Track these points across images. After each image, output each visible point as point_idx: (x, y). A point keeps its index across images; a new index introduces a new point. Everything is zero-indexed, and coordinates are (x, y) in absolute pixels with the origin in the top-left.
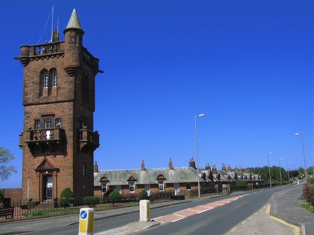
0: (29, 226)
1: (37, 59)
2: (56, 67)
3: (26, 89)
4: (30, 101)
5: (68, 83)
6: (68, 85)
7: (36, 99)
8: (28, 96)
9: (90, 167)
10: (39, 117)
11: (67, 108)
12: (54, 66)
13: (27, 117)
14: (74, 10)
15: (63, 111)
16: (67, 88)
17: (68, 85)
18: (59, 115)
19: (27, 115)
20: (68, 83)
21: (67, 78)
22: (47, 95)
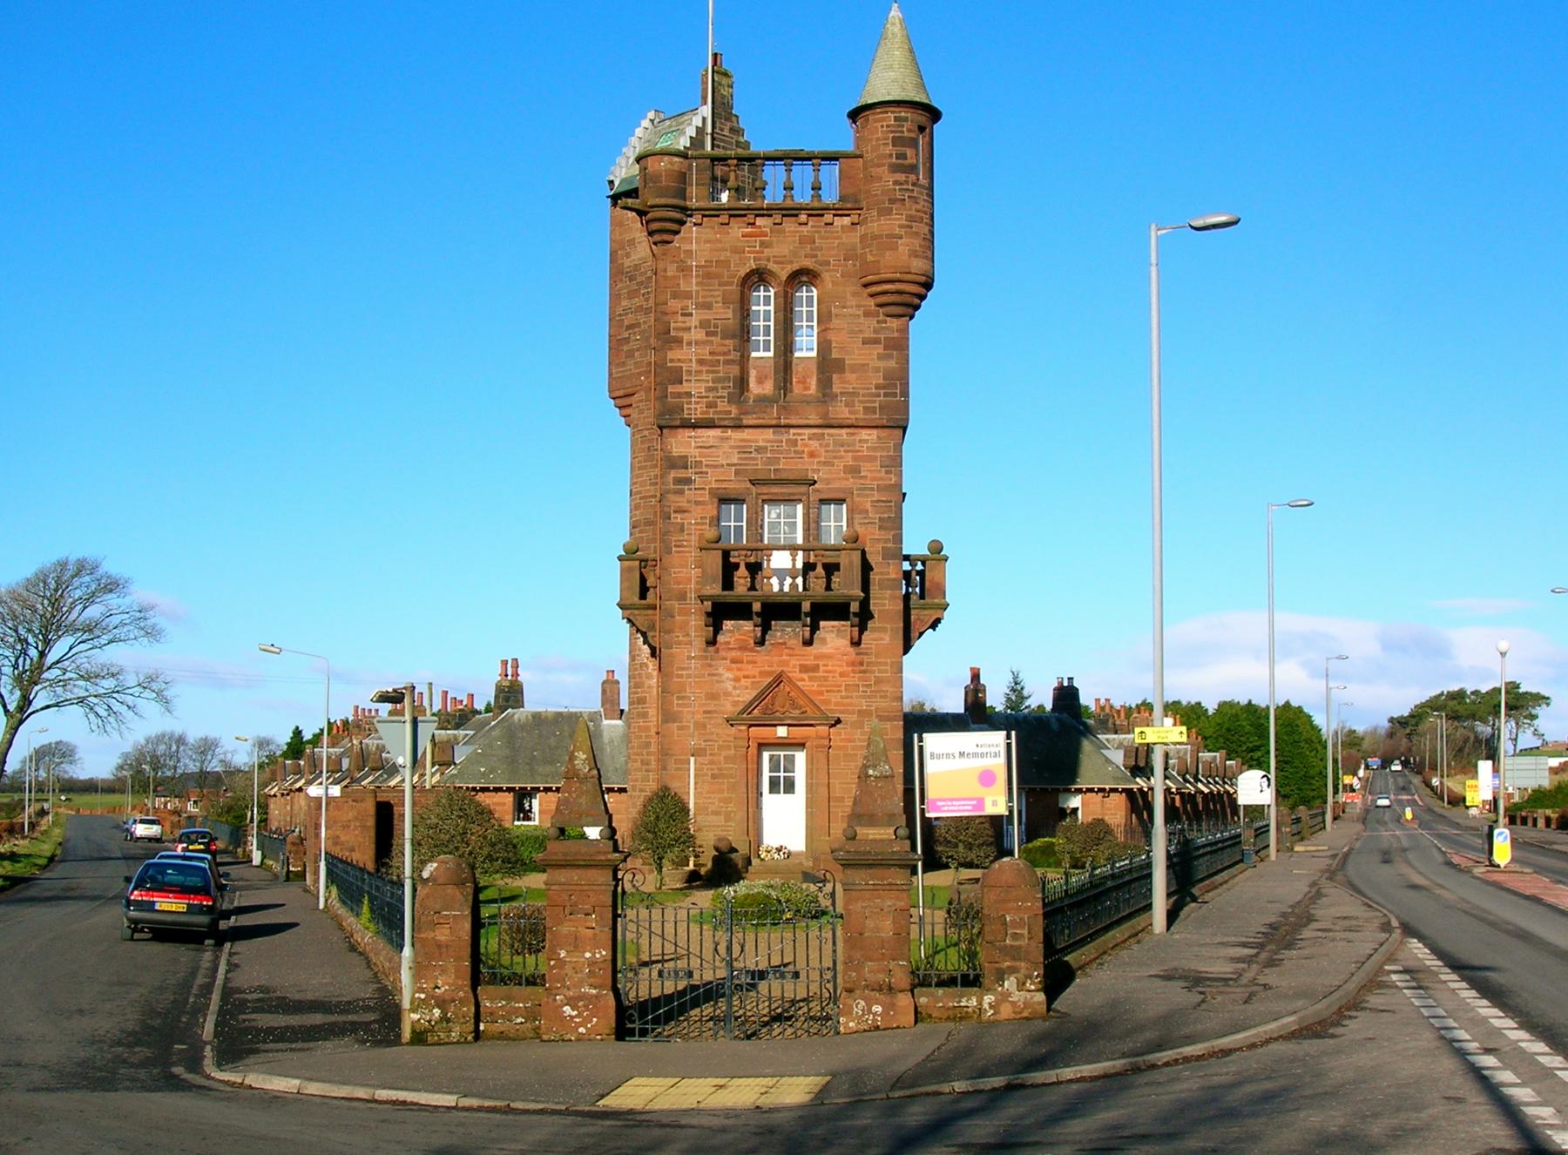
0: (1076, 1129)
1: (724, 219)
2: (818, 268)
3: (670, 355)
4: (695, 410)
5: (880, 349)
6: (880, 357)
7: (723, 405)
8: (685, 387)
9: (956, 716)
10: (736, 485)
11: (871, 459)
12: (808, 263)
13: (678, 481)
14: (895, 13)
15: (854, 471)
16: (877, 370)
17: (880, 357)
18: (836, 485)
19: (673, 474)
20: (880, 349)
21: (873, 322)
22: (768, 388)
